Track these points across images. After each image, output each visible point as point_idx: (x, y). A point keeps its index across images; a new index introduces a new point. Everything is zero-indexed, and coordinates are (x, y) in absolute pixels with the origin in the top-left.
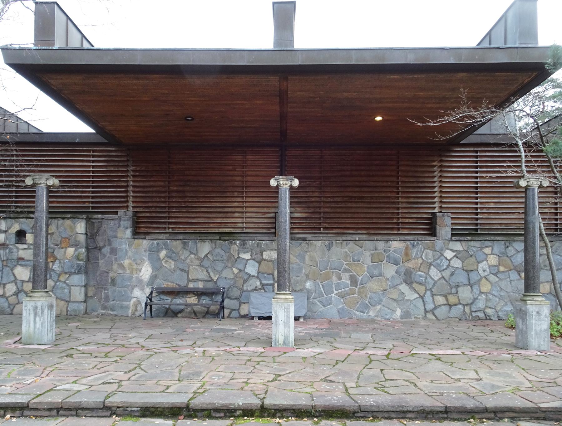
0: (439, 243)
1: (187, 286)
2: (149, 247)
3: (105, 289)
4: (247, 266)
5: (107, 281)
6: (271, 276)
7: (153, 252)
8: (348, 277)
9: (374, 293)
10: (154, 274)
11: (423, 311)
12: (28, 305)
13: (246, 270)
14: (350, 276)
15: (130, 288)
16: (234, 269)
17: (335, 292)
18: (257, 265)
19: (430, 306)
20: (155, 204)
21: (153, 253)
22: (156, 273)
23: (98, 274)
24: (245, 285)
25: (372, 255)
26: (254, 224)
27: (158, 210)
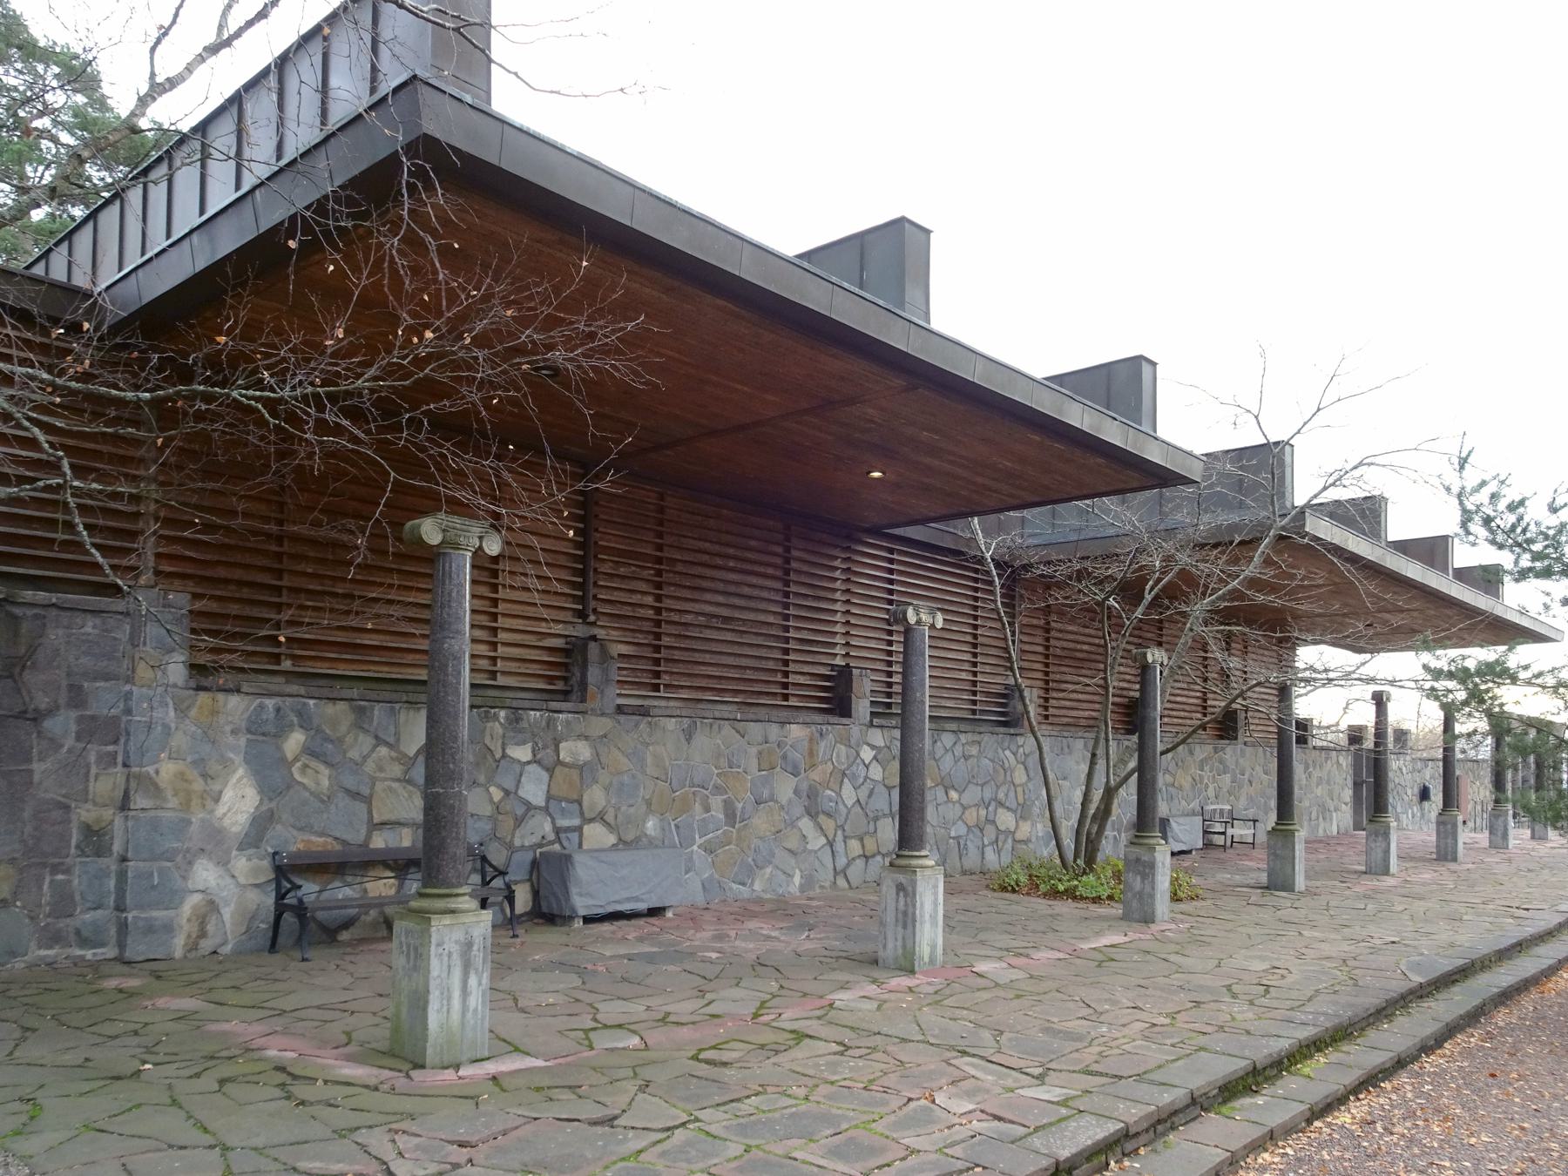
0: (855, 731)
1: (365, 844)
2: (249, 719)
3: (55, 869)
4: (523, 779)
5: (64, 838)
6: (576, 806)
7: (264, 734)
8: (721, 805)
9: (761, 838)
10: (264, 808)
11: (832, 872)
12: (446, 939)
13: (521, 793)
14: (725, 801)
15: (179, 858)
16: (492, 789)
17: (699, 841)
18: (545, 776)
19: (842, 861)
20: (238, 574)
21: (261, 738)
22: (273, 805)
23: (26, 815)
24: (517, 834)
25: (760, 753)
26: (517, 664)
27: (246, 593)
